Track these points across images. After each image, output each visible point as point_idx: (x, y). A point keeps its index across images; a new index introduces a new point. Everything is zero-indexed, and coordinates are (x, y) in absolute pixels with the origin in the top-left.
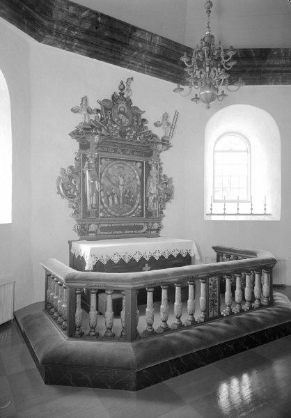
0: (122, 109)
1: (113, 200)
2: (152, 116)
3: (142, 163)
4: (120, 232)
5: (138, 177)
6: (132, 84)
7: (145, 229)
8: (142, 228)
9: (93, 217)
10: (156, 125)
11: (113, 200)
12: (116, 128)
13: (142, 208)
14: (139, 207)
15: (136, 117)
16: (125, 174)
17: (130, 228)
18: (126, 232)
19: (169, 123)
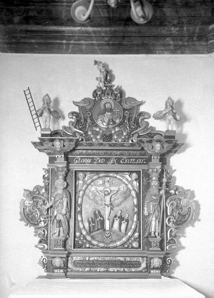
0: (108, 106)
1: (120, 225)
2: (152, 106)
3: (138, 173)
4: (102, 269)
5: (133, 193)
6: (75, 101)
7: (144, 265)
8: (139, 264)
9: (155, 249)
10: (157, 117)
11: (120, 225)
12: (99, 132)
13: (140, 235)
14: (136, 234)
15: (130, 115)
16: (106, 193)
17: (122, 264)
18: (111, 269)
19: (174, 110)
